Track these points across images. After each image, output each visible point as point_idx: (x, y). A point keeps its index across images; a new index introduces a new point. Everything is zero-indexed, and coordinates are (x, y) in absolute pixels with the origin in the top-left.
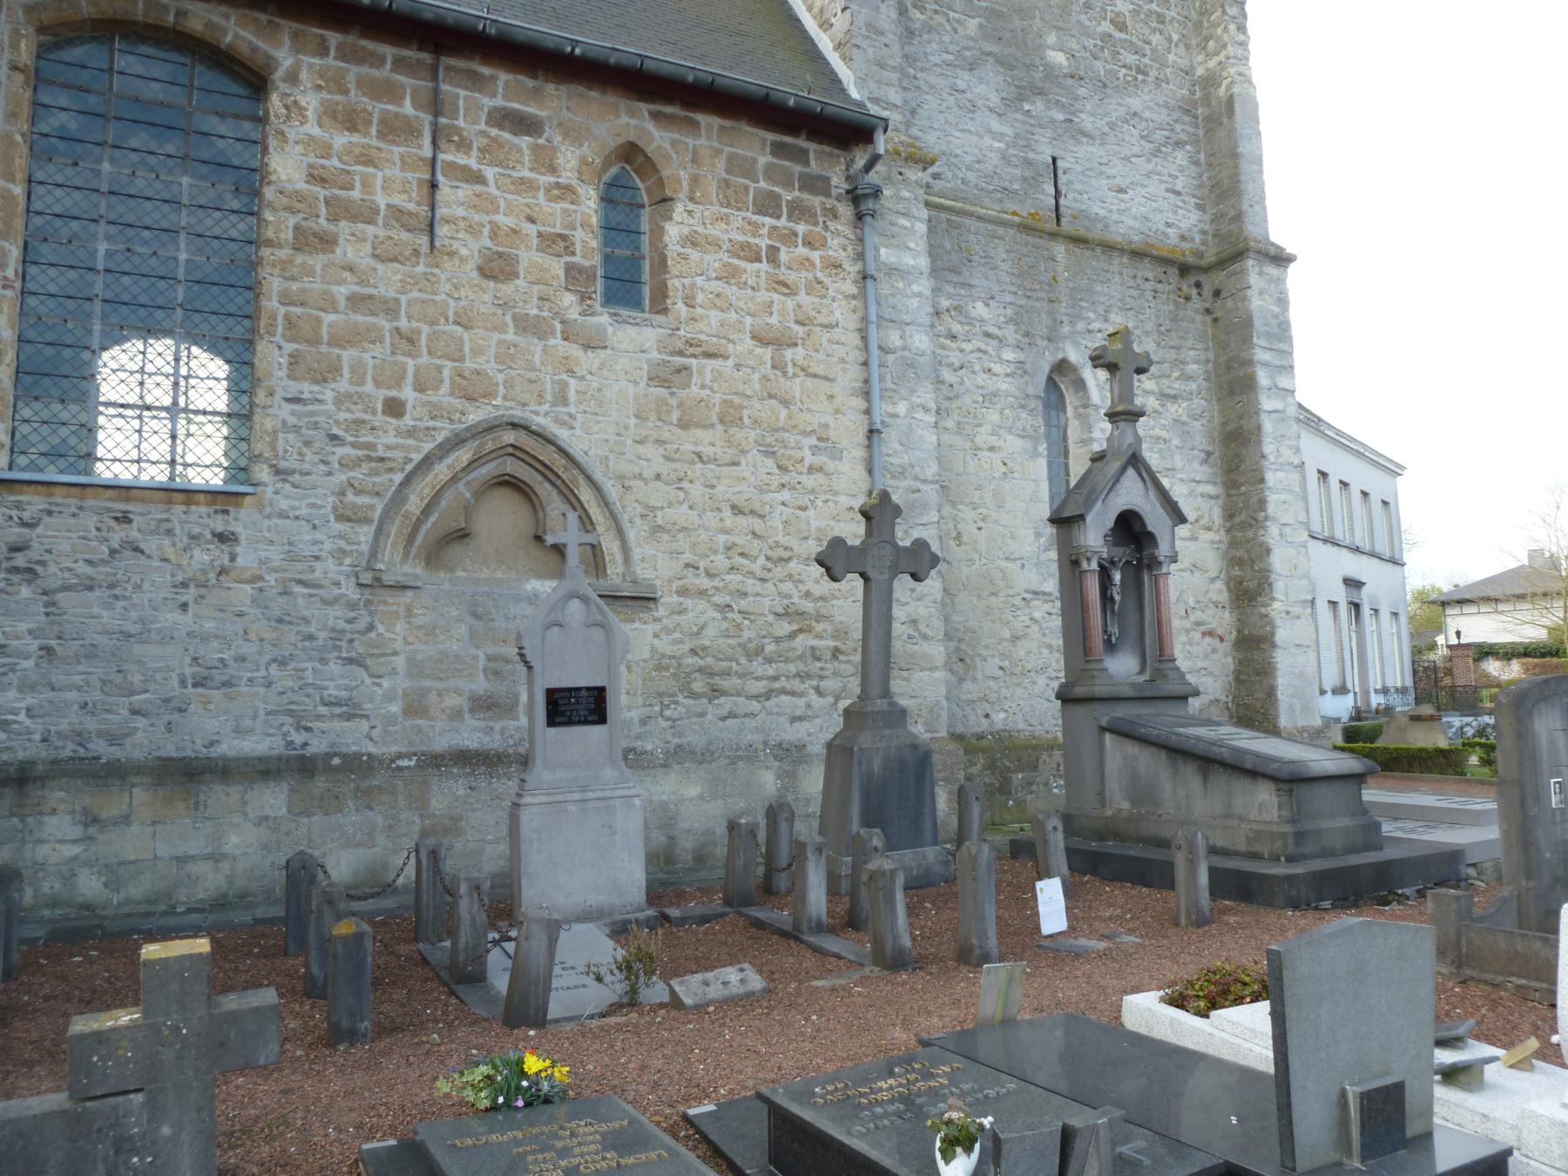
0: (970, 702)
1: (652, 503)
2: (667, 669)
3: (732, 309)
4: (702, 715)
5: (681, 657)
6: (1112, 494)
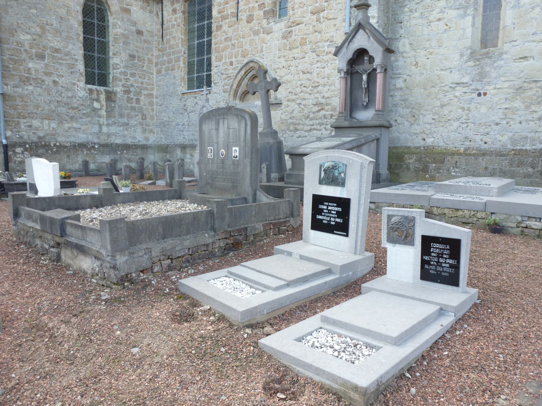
0: (416, 134)
1: (282, 75)
2: (284, 123)
3: (305, 6)
4: (292, 136)
5: (287, 120)
6: (351, 43)
